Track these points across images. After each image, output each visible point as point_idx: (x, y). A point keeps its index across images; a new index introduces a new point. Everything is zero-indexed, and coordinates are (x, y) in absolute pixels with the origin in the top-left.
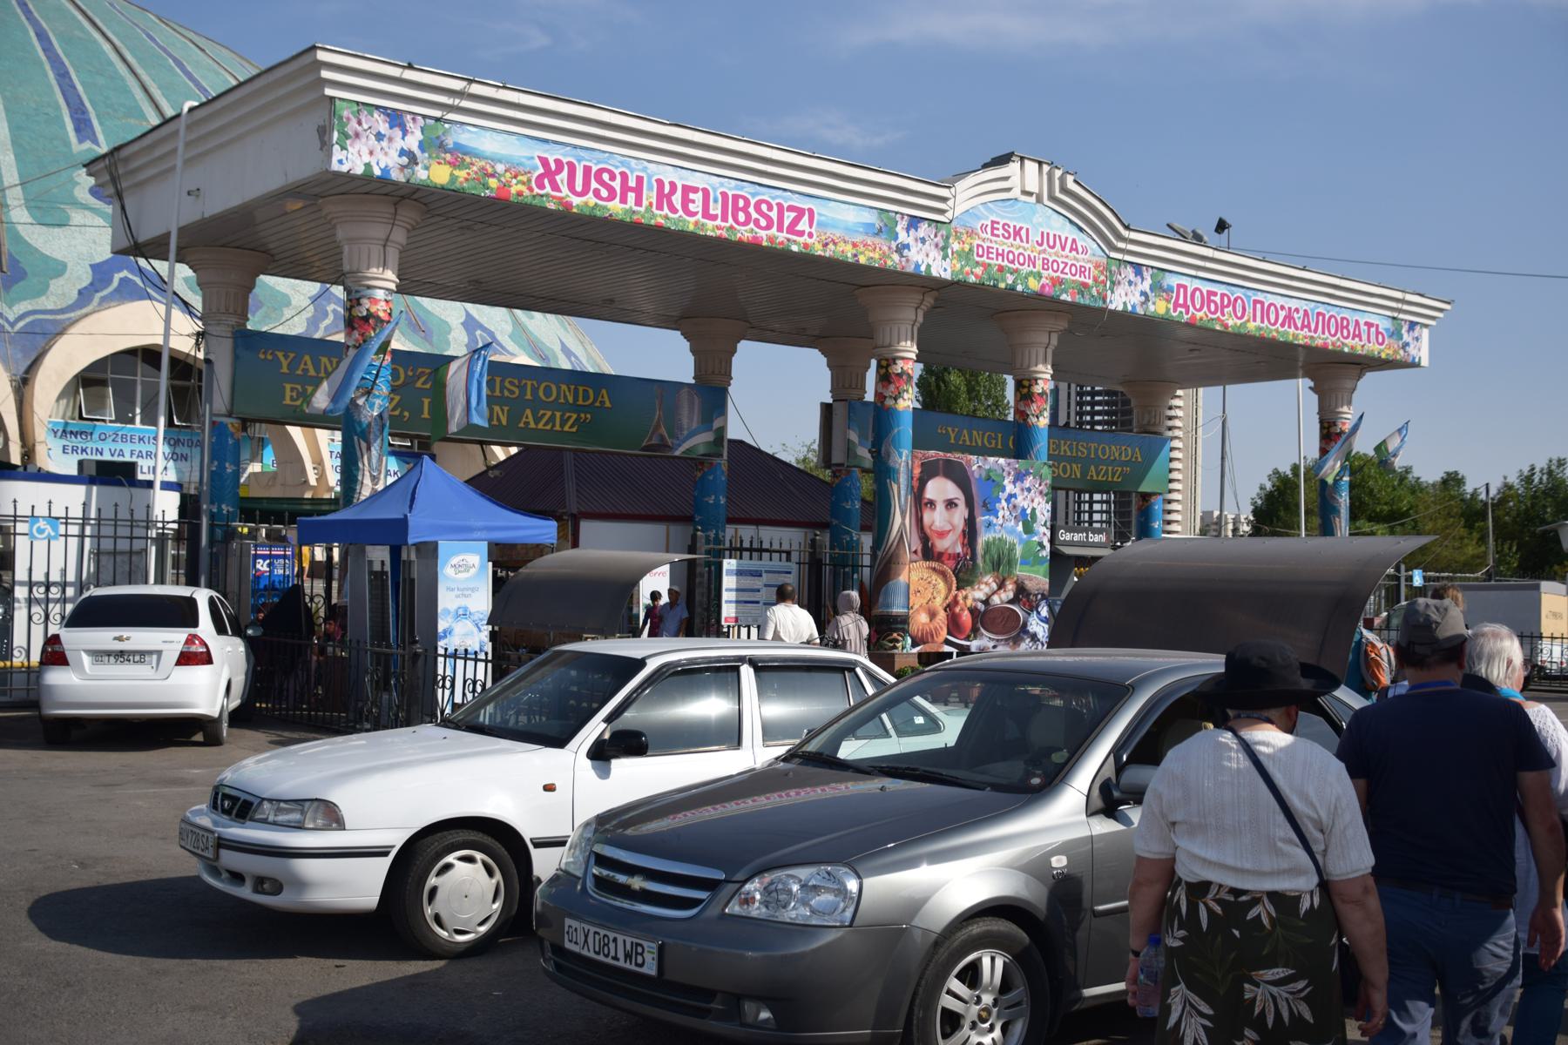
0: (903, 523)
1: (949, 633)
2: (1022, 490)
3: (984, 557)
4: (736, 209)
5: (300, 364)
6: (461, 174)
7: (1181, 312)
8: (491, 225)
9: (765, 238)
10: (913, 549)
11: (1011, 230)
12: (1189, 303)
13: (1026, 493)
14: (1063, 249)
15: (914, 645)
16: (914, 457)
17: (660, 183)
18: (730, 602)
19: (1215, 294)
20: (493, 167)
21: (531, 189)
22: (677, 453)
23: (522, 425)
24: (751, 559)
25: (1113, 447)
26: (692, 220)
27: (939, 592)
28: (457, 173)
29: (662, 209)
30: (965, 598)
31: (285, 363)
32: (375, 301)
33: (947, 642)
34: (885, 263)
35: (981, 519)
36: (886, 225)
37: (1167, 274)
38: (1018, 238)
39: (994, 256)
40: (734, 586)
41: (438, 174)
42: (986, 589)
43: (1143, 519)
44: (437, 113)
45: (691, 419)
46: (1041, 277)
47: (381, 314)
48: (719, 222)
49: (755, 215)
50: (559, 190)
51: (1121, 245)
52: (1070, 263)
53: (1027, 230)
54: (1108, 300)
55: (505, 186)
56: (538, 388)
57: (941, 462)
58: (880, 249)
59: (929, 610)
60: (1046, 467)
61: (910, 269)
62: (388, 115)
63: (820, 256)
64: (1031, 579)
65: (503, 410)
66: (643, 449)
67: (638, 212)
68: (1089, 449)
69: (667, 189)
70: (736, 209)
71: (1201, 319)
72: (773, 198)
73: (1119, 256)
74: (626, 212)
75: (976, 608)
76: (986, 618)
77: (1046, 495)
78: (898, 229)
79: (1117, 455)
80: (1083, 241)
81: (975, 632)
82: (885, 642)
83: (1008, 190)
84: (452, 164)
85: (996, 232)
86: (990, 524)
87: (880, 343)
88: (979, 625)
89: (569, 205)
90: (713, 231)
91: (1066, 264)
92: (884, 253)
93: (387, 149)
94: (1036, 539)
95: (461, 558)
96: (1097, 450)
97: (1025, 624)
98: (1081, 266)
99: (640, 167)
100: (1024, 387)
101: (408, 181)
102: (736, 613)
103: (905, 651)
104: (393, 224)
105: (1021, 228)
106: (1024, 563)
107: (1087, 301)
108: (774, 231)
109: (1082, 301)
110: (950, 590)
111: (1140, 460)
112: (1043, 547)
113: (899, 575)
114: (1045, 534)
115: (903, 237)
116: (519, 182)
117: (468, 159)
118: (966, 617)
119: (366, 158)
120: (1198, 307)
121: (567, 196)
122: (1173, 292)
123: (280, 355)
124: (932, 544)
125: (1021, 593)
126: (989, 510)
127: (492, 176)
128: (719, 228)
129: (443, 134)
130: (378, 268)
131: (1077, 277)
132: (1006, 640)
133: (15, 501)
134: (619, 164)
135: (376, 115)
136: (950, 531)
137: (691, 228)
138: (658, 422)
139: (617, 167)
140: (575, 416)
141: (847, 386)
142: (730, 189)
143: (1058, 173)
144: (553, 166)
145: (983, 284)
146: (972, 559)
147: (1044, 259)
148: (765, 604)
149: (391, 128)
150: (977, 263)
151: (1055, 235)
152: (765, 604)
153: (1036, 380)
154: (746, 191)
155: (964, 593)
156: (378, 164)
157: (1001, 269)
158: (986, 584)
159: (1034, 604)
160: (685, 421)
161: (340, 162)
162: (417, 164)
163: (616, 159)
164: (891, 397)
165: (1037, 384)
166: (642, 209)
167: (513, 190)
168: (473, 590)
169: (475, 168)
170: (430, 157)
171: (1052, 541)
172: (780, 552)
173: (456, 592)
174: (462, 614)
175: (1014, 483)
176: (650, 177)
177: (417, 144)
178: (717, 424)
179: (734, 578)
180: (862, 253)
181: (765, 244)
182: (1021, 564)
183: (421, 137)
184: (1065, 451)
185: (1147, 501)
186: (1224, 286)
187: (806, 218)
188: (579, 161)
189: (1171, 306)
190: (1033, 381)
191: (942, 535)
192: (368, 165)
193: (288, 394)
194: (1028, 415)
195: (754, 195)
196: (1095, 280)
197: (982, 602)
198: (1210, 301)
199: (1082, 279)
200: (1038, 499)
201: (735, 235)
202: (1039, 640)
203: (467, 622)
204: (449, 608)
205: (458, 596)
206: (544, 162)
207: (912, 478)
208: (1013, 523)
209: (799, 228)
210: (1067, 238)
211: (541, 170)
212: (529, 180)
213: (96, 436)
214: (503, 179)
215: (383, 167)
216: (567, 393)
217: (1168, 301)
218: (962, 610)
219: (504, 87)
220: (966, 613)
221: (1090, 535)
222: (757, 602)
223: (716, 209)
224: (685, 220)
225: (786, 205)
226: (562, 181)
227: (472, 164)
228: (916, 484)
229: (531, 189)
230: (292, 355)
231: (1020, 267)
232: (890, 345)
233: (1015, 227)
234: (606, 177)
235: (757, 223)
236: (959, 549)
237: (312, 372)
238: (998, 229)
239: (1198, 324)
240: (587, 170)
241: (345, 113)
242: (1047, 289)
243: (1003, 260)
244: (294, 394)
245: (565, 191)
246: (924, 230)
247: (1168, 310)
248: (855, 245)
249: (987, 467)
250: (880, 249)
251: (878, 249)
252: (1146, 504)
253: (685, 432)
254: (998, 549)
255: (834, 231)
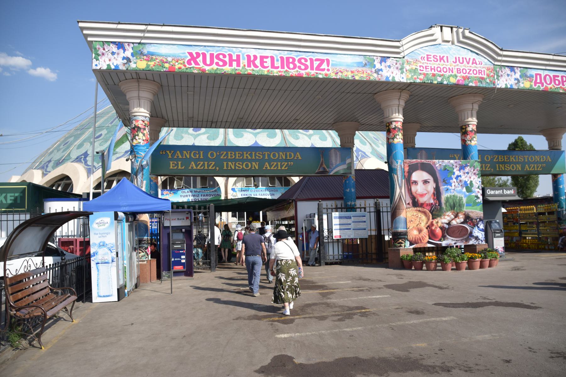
0: (401, 192)
1: (430, 238)
2: (464, 173)
3: (446, 204)
4: (288, 63)
5: (176, 154)
6: (151, 63)
7: (539, 86)
8: (374, 125)
9: (304, 74)
10: (407, 202)
11: (438, 58)
12: (543, 81)
13: (466, 175)
14: (468, 63)
15: (411, 244)
16: (404, 163)
17: (249, 56)
18: (337, 229)
19: (558, 76)
20: (166, 59)
21: (185, 66)
22: (331, 174)
23: (264, 168)
24: (361, 211)
25: (536, 157)
26: (266, 70)
27: (423, 221)
28: (149, 63)
29: (250, 67)
30: (437, 222)
31: (170, 154)
32: (137, 121)
33: (429, 242)
34: (370, 78)
35: (442, 188)
36: (368, 62)
37: (529, 70)
38: (442, 61)
39: (430, 70)
40: (338, 223)
41: (142, 65)
42: (449, 218)
43: (555, 185)
44: (138, 41)
45: (336, 160)
46: (457, 77)
47: (140, 126)
48: (280, 69)
49: (298, 64)
50: (199, 64)
51: (500, 58)
52: (472, 69)
53: (447, 57)
54: (496, 84)
55: (172, 66)
56: (270, 154)
57: (419, 164)
58: (366, 72)
59: (418, 229)
60: (476, 163)
61: (384, 79)
62: (117, 45)
63: (334, 78)
64: (472, 212)
65: (256, 164)
66: (316, 174)
67: (239, 70)
68: (524, 158)
69: (252, 58)
70: (288, 63)
71: (551, 88)
72: (307, 57)
73: (499, 64)
74: (232, 70)
75: (443, 227)
76: (448, 231)
77: (478, 174)
78: (376, 63)
79: (538, 160)
80: (478, 59)
81: (444, 237)
82: (396, 244)
83: (435, 40)
84: (147, 60)
85: (429, 59)
86: (447, 189)
87: (385, 116)
88: (446, 234)
89: (204, 70)
90: (277, 73)
91: (471, 70)
92: (369, 74)
93: (117, 58)
94: (474, 194)
95: (101, 219)
96: (528, 158)
97: (471, 233)
98: (479, 70)
99: (238, 51)
100: (463, 129)
101: (127, 69)
102: (340, 234)
103: (406, 248)
104: (139, 90)
105: (443, 57)
106: (468, 205)
107: (484, 85)
108: (309, 70)
109: (481, 85)
110: (429, 219)
111: (550, 161)
112: (478, 198)
113: (400, 214)
114: (478, 192)
115: (378, 66)
116: (179, 64)
117: (154, 57)
118: (438, 231)
119: (108, 62)
120: (548, 83)
121: (203, 66)
122: (533, 77)
123: (168, 152)
124: (417, 200)
125: (468, 219)
126: (447, 183)
127: (166, 62)
128: (280, 72)
129: (142, 49)
130: (137, 108)
131: (478, 75)
132: (461, 240)
133: (50, 208)
134: (227, 51)
135: (111, 45)
136: (427, 193)
137: (266, 73)
138: (322, 162)
139: (226, 52)
140: (286, 163)
141: (406, 142)
142: (285, 55)
143: (461, 31)
144: (195, 55)
145: (425, 83)
146: (439, 205)
147: (457, 69)
148: (353, 229)
149: (118, 49)
150: (420, 73)
151: (463, 58)
152: (353, 229)
153: (468, 125)
154: (293, 55)
155: (436, 220)
156: (113, 64)
157: (434, 75)
158: (448, 216)
159: (476, 223)
160: (334, 161)
161: (96, 65)
162: (131, 62)
163: (226, 49)
164: (391, 138)
165: (469, 127)
166: (240, 68)
167: (177, 67)
168: (107, 234)
169: (158, 60)
170: (137, 58)
171: (483, 194)
172: (361, 208)
173: (99, 235)
174: (103, 245)
175: (459, 170)
176: (243, 55)
177: (131, 54)
178: (348, 161)
179: (338, 220)
180: (356, 75)
181: (304, 76)
182: (466, 206)
183: (132, 51)
184: (512, 160)
185: (556, 177)
186: (563, 72)
187: (325, 63)
188: (208, 52)
189: (533, 84)
190: (467, 126)
191: (422, 195)
192: (109, 65)
193: (171, 165)
194: (466, 141)
195: (297, 56)
196: (488, 75)
197: (447, 224)
198: (555, 80)
199: (480, 75)
200: (473, 177)
201: (289, 74)
202: (479, 239)
203: (105, 248)
204: (96, 242)
205: (100, 237)
206: (191, 54)
207: (404, 172)
208: (460, 188)
209: (322, 67)
210: (470, 59)
211: (189, 58)
212: (184, 62)
213: (249, 191)
214: (171, 63)
215: (115, 65)
216: (282, 155)
217: (531, 81)
218: (436, 228)
219: (164, 25)
220: (438, 229)
221: (505, 191)
222: (350, 229)
223: (278, 64)
224: (262, 70)
225: (314, 59)
226: (200, 61)
227: (157, 59)
228: (406, 174)
229: (185, 66)
230: (172, 152)
231: (444, 73)
232: (389, 117)
233: (440, 56)
234: (221, 57)
235: (300, 68)
236: (432, 201)
237: (180, 157)
238: (431, 58)
239: (549, 90)
240: (212, 55)
241: (97, 47)
242: (461, 82)
243: (435, 71)
244: (174, 165)
245: (202, 65)
246: (389, 62)
247: (531, 86)
248: (352, 72)
249: (444, 164)
250: (366, 72)
251: (365, 73)
252: (556, 179)
253: (334, 166)
254: (453, 200)
255: (341, 67)
